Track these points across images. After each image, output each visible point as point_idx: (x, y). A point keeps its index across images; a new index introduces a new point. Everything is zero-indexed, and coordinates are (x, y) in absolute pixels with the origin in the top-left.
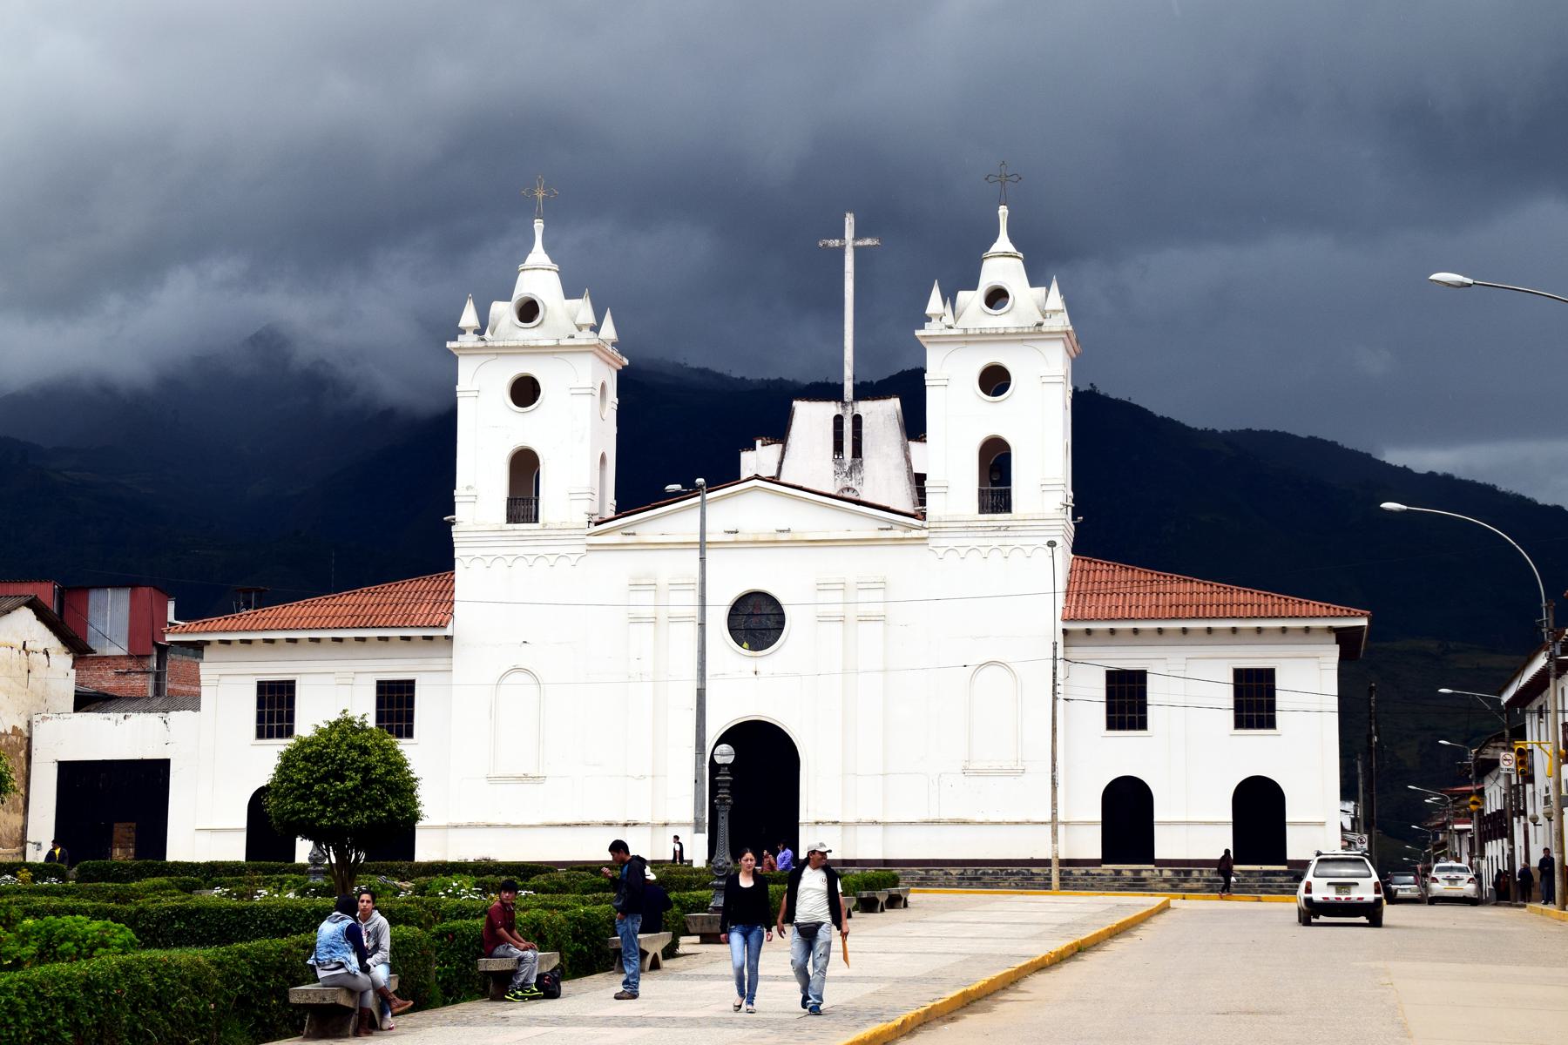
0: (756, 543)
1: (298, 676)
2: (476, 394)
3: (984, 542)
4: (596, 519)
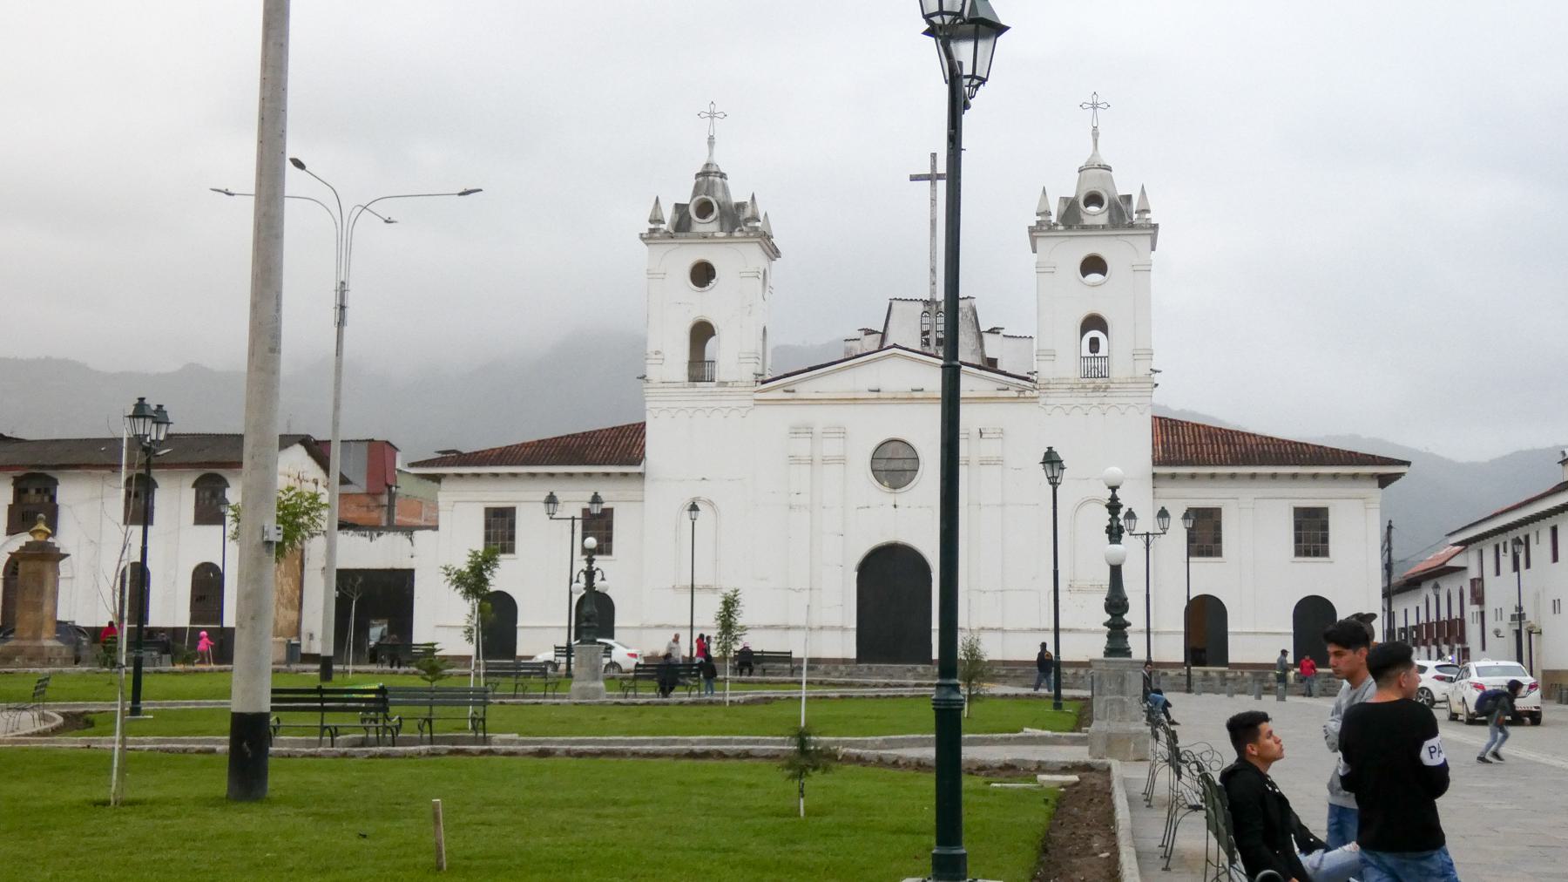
0: (895, 399)
1: (1333, 501)
2: (662, 276)
3: (710, 404)
4: (760, 378)
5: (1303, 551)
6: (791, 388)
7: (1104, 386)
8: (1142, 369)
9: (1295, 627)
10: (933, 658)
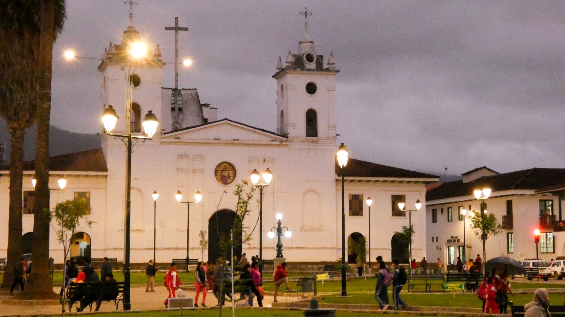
0: (226, 144)
5: (399, 214)
6: (177, 137)
7: (316, 141)
8: (332, 134)
9: (392, 247)
10: (367, 261)
